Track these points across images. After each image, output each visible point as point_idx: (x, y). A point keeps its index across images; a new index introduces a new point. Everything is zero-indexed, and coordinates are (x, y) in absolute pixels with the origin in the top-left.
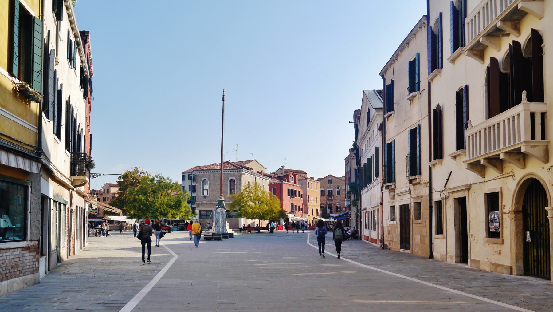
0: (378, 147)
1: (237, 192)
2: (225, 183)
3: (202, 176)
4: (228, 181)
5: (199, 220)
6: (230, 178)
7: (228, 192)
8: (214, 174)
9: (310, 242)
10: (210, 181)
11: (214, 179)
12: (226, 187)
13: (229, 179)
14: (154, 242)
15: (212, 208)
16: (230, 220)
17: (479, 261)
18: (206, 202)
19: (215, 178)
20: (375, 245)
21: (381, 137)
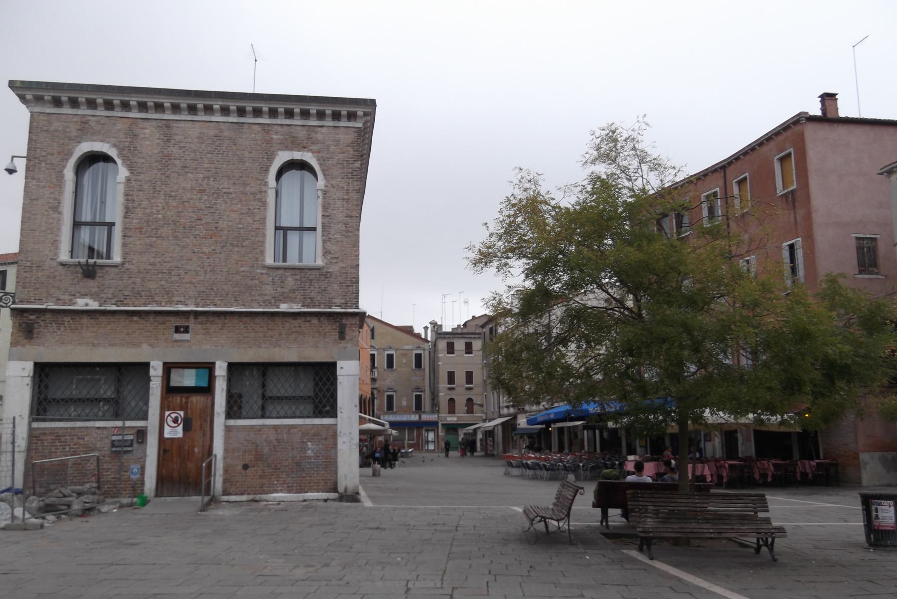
0: (472, 372)
1: (679, 188)
2: (245, 184)
3: (73, 131)
4: (267, 171)
5: (31, 430)
6: (283, 157)
7: (262, 243)
8: (168, 124)
9: (793, 185)
10: (131, 168)
11: (169, 157)
12: (250, 213)
13: (271, 158)
14: (9, 480)
15: (137, 345)
16: (276, 427)
17: (875, 239)
18: (94, 305)
19: (175, 150)
20: (792, 152)
21: (835, 125)
